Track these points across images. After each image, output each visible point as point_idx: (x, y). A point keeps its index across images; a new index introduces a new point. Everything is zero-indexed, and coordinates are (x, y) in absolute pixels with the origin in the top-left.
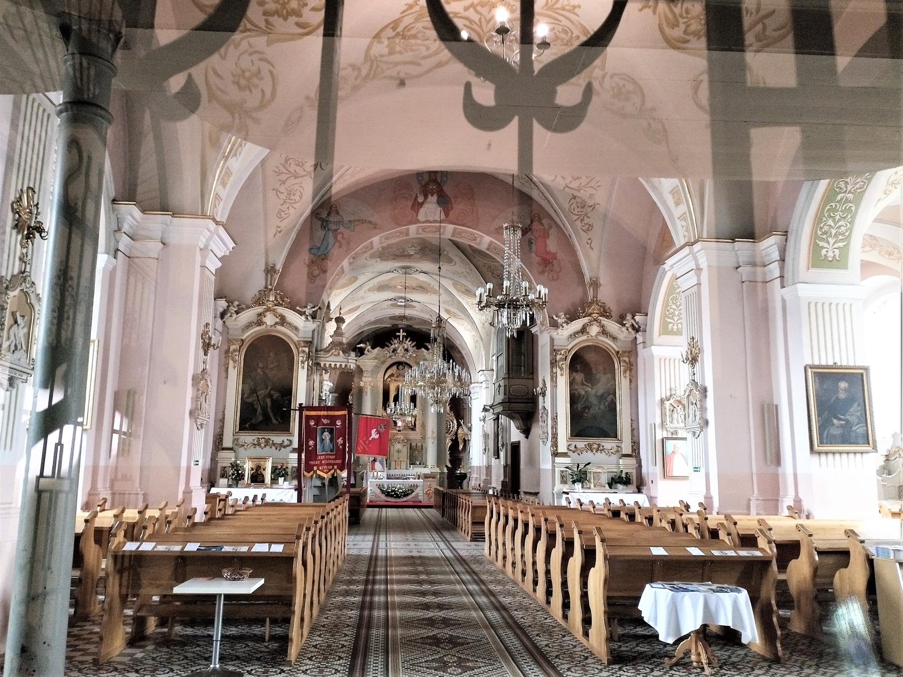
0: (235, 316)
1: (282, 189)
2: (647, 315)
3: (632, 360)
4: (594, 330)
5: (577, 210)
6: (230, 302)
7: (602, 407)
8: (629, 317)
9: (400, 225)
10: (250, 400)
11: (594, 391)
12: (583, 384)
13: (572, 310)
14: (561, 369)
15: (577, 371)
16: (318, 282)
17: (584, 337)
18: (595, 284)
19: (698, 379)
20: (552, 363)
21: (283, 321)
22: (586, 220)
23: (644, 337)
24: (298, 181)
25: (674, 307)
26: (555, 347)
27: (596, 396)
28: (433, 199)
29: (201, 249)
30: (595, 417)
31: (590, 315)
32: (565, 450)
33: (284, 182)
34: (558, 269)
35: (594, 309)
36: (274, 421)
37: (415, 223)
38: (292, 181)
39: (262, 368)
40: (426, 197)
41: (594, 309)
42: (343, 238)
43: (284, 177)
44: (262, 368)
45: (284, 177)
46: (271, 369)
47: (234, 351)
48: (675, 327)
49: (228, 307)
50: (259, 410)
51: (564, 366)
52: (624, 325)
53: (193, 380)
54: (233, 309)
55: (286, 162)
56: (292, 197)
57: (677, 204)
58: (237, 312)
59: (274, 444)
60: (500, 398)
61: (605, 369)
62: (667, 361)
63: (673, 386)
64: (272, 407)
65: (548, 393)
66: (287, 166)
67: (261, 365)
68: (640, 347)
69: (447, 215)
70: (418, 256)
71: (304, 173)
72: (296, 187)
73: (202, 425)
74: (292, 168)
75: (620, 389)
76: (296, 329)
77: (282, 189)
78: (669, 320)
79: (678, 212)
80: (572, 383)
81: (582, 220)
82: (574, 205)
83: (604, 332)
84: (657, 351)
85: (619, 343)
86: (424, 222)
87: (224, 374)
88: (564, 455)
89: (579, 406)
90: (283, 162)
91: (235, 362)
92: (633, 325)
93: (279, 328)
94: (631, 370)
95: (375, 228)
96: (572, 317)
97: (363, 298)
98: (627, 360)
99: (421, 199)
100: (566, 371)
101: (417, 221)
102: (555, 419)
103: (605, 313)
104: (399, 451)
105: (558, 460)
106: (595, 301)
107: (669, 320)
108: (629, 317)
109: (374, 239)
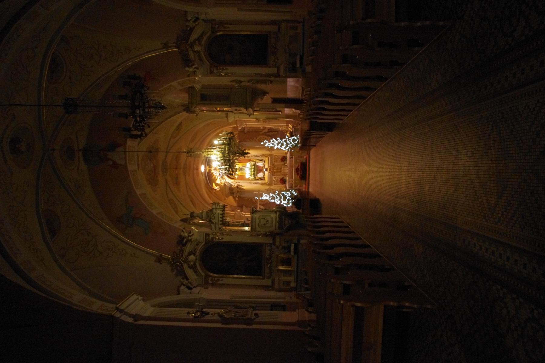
17: (202, 54)
32: (270, 280)
37: (126, 166)
47: (212, 280)
49: (184, 285)
54: (185, 282)
58: (187, 279)
60: (243, 110)
65: (239, 79)
76: (203, 33)
80: (233, 64)
83: (199, 39)
88: (273, 282)
91: (218, 280)
93: (197, 254)
99: (110, 163)
101: (126, 166)
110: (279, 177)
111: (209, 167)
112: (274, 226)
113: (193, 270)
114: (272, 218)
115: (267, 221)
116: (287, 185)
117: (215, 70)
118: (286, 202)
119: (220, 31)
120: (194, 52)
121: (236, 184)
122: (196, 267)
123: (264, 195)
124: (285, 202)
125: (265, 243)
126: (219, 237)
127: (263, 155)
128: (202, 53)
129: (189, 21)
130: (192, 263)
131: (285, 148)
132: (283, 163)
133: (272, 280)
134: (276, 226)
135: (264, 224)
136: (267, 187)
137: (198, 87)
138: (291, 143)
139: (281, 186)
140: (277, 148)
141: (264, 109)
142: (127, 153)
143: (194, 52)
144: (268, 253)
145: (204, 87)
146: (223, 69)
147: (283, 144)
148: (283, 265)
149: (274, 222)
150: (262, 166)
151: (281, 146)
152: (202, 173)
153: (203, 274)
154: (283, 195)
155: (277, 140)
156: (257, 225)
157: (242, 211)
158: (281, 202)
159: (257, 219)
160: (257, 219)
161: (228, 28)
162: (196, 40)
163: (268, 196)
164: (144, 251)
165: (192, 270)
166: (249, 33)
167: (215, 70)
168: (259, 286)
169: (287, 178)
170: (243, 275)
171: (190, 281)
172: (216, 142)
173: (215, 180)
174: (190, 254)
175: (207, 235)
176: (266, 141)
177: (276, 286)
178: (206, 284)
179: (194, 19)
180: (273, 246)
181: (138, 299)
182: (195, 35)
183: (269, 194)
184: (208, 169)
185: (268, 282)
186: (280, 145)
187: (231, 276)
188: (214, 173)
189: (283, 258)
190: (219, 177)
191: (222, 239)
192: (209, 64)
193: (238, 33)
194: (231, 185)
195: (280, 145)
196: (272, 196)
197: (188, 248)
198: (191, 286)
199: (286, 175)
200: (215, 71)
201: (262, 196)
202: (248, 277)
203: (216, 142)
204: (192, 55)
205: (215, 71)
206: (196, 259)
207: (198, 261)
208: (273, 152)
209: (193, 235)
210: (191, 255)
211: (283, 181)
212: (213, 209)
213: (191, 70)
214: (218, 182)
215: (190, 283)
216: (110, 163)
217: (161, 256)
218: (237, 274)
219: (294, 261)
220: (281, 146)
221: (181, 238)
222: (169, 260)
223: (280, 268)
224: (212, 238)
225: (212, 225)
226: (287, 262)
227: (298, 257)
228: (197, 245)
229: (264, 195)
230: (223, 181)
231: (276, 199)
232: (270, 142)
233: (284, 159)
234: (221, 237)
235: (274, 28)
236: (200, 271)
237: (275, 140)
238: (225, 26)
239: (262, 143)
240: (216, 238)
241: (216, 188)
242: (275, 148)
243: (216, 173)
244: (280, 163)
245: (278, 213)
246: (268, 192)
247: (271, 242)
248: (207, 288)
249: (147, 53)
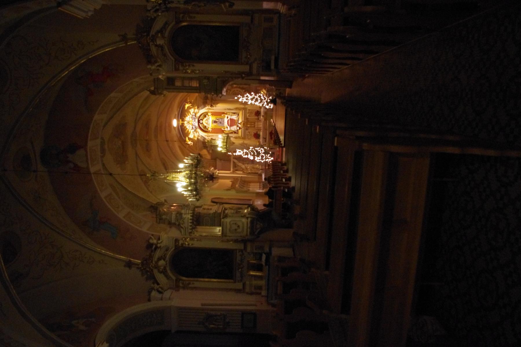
0: (161, 286)
17: (166, 48)
32: (241, 284)
47: (183, 284)
58: (158, 284)
83: (161, 31)
86: (88, 164)
88: (244, 285)
91: (189, 284)
98: (181, 15)
105: (255, 71)
110: (253, 131)
111: (182, 121)
112: (245, 230)
113: (164, 274)
114: (243, 223)
115: (239, 226)
116: (261, 140)
117: (180, 66)
118: (260, 158)
119: (184, 21)
120: (156, 46)
121: (210, 138)
122: (166, 271)
123: (238, 151)
124: (259, 158)
125: (236, 250)
126: (188, 243)
127: (236, 109)
128: (166, 47)
129: (149, 11)
130: (162, 268)
131: (260, 103)
132: (256, 117)
134: (247, 232)
135: (236, 230)
136: (241, 141)
138: (265, 99)
139: (254, 141)
140: (251, 104)
143: (156, 45)
144: (239, 258)
146: (189, 66)
147: (257, 100)
148: (254, 270)
149: (245, 228)
150: (235, 119)
151: (255, 102)
152: (174, 127)
153: (174, 278)
154: (257, 151)
155: (251, 95)
156: (228, 230)
157: (215, 169)
158: (254, 158)
159: (228, 224)
160: (228, 224)
161: (194, 17)
162: (158, 32)
163: (242, 152)
164: (113, 258)
166: (218, 24)
167: (180, 66)
168: (231, 290)
169: (261, 134)
170: (214, 278)
171: (161, 286)
172: (181, 166)
173: (188, 134)
174: (159, 259)
175: (177, 240)
176: (239, 96)
177: (247, 290)
178: (177, 288)
180: (244, 251)
182: (157, 26)
183: (243, 150)
184: (181, 122)
185: (239, 286)
186: (254, 100)
188: (187, 127)
189: (255, 263)
190: (192, 131)
191: (192, 244)
192: (174, 60)
193: (206, 24)
194: (205, 139)
195: (254, 100)
196: (246, 152)
197: (158, 254)
198: (162, 291)
199: (259, 130)
200: (181, 68)
201: (235, 152)
202: (219, 280)
203: (181, 166)
204: (154, 49)
205: (181, 68)
206: (166, 264)
207: (168, 265)
208: (246, 106)
210: (160, 260)
211: (257, 136)
213: (153, 67)
214: (191, 136)
215: (161, 288)
216: (72, 165)
217: (130, 261)
218: (208, 278)
219: (266, 268)
220: (255, 102)
221: (150, 246)
222: (138, 265)
223: (251, 273)
224: (182, 244)
225: (182, 230)
226: (259, 268)
227: (269, 267)
228: (167, 250)
229: (238, 151)
230: (196, 135)
231: (249, 155)
232: (243, 97)
233: (258, 113)
234: (191, 242)
235: (246, 19)
236: (171, 275)
237: (249, 95)
238: (191, 15)
239: (236, 98)
240: (185, 244)
241: (189, 143)
242: (249, 103)
243: (189, 127)
244: (254, 117)
245: (249, 220)
246: (242, 147)
247: (242, 248)
248: (178, 291)
249: (102, 47)
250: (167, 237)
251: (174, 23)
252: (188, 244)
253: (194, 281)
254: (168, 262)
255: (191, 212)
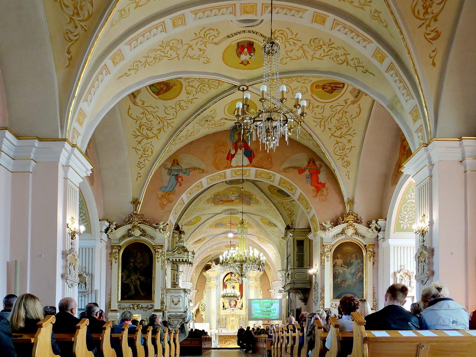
0: (114, 231)
1: (139, 147)
2: (386, 220)
3: (375, 250)
4: (350, 232)
5: (339, 152)
6: (111, 223)
7: (354, 280)
8: (374, 222)
9: (219, 170)
10: (126, 282)
11: (349, 270)
12: (342, 266)
13: (335, 219)
14: (328, 257)
15: (338, 258)
16: (166, 208)
17: (343, 237)
18: (351, 202)
19: (426, 244)
20: (321, 254)
21: (144, 233)
22: (346, 159)
23: (384, 234)
24: (150, 140)
25: (405, 213)
26: (324, 244)
27: (350, 273)
28: (240, 152)
29: (63, 166)
30: (349, 286)
31: (347, 222)
33: (140, 143)
34: (326, 194)
35: (350, 218)
36: (142, 294)
38: (145, 141)
39: (133, 263)
40: (236, 151)
41: (350, 218)
42: (182, 180)
43: (139, 138)
44: (133, 263)
45: (139, 138)
46: (139, 263)
47: (115, 252)
48: (405, 226)
49: (110, 225)
50: (132, 287)
51: (329, 255)
52: (370, 228)
53: (63, 254)
55: (140, 127)
56: (146, 153)
57: (415, 120)
58: (115, 229)
59: (142, 308)
61: (356, 256)
62: (399, 248)
63: (402, 264)
64: (140, 286)
66: (141, 131)
67: (132, 261)
68: (380, 242)
69: (251, 161)
70: (237, 201)
71: (153, 135)
72: (148, 145)
73: (72, 285)
74: (145, 132)
75: (366, 277)
77: (139, 147)
78: (401, 222)
79: (413, 127)
80: (334, 266)
81: (342, 159)
82: (337, 149)
83: (357, 233)
84: (392, 242)
85: (366, 240)
86: (235, 167)
87: (110, 267)
89: (339, 280)
90: (138, 128)
91: (116, 259)
92: (376, 227)
93: (142, 238)
94: (374, 257)
95: (203, 172)
96: (336, 223)
97: (207, 232)
98: (371, 250)
100: (330, 259)
101: (231, 167)
102: (323, 290)
103: (358, 220)
104: (233, 321)
106: (351, 213)
107: (401, 222)
108: (374, 222)
109: (202, 180)
133: (116, 311)
135: (173, 301)
137: (310, 236)
141: (290, 302)
142: (242, 168)
145: (310, 241)
165: (125, 233)
171: (114, 231)
178: (112, 247)
179: (379, 228)
181: (87, 170)
187: (120, 271)
191: (158, 261)
207: (136, 238)
209: (161, 232)
212: (188, 252)
215: (111, 231)
216: (233, 152)
217: (139, 203)
224: (158, 252)
250: (162, 238)
251: (153, 244)
252: (158, 258)
253: (119, 262)
254: (138, 238)
255: (190, 261)
